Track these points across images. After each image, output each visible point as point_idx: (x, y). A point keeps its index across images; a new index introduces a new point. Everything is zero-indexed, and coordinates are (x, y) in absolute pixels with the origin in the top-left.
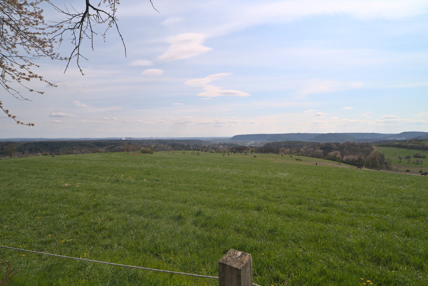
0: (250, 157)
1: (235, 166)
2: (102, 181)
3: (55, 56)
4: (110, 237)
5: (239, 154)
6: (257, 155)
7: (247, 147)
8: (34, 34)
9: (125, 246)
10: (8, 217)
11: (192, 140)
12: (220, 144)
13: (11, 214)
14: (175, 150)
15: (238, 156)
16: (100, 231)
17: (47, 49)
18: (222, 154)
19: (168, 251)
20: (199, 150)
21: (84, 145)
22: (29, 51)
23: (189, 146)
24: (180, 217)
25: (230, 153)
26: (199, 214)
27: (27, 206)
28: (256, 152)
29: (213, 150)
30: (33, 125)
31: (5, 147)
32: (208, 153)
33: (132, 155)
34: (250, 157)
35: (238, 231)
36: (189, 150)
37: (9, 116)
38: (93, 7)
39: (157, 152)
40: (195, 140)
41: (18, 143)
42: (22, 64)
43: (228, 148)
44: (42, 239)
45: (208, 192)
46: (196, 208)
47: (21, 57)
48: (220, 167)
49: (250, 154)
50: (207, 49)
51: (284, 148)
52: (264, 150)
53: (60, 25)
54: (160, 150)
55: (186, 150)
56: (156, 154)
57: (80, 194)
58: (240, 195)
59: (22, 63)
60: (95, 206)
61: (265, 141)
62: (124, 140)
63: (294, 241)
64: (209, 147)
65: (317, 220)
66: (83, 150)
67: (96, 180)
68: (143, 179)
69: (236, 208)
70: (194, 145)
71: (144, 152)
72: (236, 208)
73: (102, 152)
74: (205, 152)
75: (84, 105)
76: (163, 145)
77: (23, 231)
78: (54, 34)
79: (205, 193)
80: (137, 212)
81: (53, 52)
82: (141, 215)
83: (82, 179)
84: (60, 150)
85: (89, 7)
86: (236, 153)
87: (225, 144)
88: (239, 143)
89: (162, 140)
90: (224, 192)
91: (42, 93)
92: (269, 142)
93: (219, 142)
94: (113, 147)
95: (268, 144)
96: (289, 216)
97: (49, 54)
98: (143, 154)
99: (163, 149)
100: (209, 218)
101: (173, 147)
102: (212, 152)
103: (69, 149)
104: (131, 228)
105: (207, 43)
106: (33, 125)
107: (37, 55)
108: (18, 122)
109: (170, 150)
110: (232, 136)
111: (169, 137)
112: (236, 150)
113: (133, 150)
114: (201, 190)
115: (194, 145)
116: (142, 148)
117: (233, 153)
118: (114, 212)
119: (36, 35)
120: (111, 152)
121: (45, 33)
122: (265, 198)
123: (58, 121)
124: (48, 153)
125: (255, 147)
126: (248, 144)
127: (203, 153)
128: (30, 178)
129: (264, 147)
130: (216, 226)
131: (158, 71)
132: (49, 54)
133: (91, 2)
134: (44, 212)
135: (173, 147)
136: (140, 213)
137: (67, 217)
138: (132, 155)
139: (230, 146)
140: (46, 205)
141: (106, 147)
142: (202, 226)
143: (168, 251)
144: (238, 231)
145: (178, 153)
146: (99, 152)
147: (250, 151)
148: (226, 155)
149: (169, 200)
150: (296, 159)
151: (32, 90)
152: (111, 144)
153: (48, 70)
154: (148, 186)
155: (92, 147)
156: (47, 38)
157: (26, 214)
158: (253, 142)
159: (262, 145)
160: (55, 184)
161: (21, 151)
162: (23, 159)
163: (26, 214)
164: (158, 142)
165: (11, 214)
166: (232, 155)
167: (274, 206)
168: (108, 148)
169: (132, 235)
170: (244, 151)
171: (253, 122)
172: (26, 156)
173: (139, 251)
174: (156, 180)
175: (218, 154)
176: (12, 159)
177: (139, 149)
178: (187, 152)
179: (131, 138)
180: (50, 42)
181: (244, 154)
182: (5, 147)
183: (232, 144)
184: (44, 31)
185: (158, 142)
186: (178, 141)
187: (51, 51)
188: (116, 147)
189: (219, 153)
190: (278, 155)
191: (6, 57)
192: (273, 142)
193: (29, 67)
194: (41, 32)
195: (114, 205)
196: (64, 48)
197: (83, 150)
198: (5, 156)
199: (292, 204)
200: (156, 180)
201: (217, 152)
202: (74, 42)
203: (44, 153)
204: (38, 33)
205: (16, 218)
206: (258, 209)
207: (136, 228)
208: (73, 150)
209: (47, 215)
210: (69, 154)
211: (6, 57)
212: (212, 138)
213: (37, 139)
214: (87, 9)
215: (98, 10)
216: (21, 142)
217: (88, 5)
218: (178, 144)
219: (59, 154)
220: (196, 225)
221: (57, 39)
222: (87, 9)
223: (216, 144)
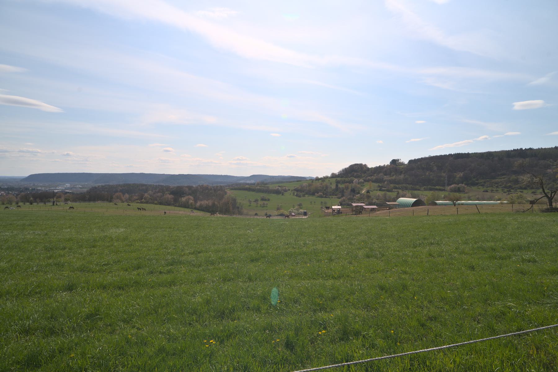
5: (42, 204)
7: (57, 193)
25: (21, 204)
35: (26, 332)
43: (17, 195)
49: (62, 204)
58: (36, 271)
61: (91, 184)
86: (35, 204)
88: (41, 187)
92: (97, 185)
95: (95, 188)
110: (26, 175)
117: (28, 204)
122: (82, 269)
126: (58, 189)
129: (89, 192)
139: (22, 191)
147: (63, 199)
158: (68, 185)
159: (85, 190)
170: (52, 200)
181: (51, 204)
183: (27, 189)
192: (103, 184)
206: (70, 288)
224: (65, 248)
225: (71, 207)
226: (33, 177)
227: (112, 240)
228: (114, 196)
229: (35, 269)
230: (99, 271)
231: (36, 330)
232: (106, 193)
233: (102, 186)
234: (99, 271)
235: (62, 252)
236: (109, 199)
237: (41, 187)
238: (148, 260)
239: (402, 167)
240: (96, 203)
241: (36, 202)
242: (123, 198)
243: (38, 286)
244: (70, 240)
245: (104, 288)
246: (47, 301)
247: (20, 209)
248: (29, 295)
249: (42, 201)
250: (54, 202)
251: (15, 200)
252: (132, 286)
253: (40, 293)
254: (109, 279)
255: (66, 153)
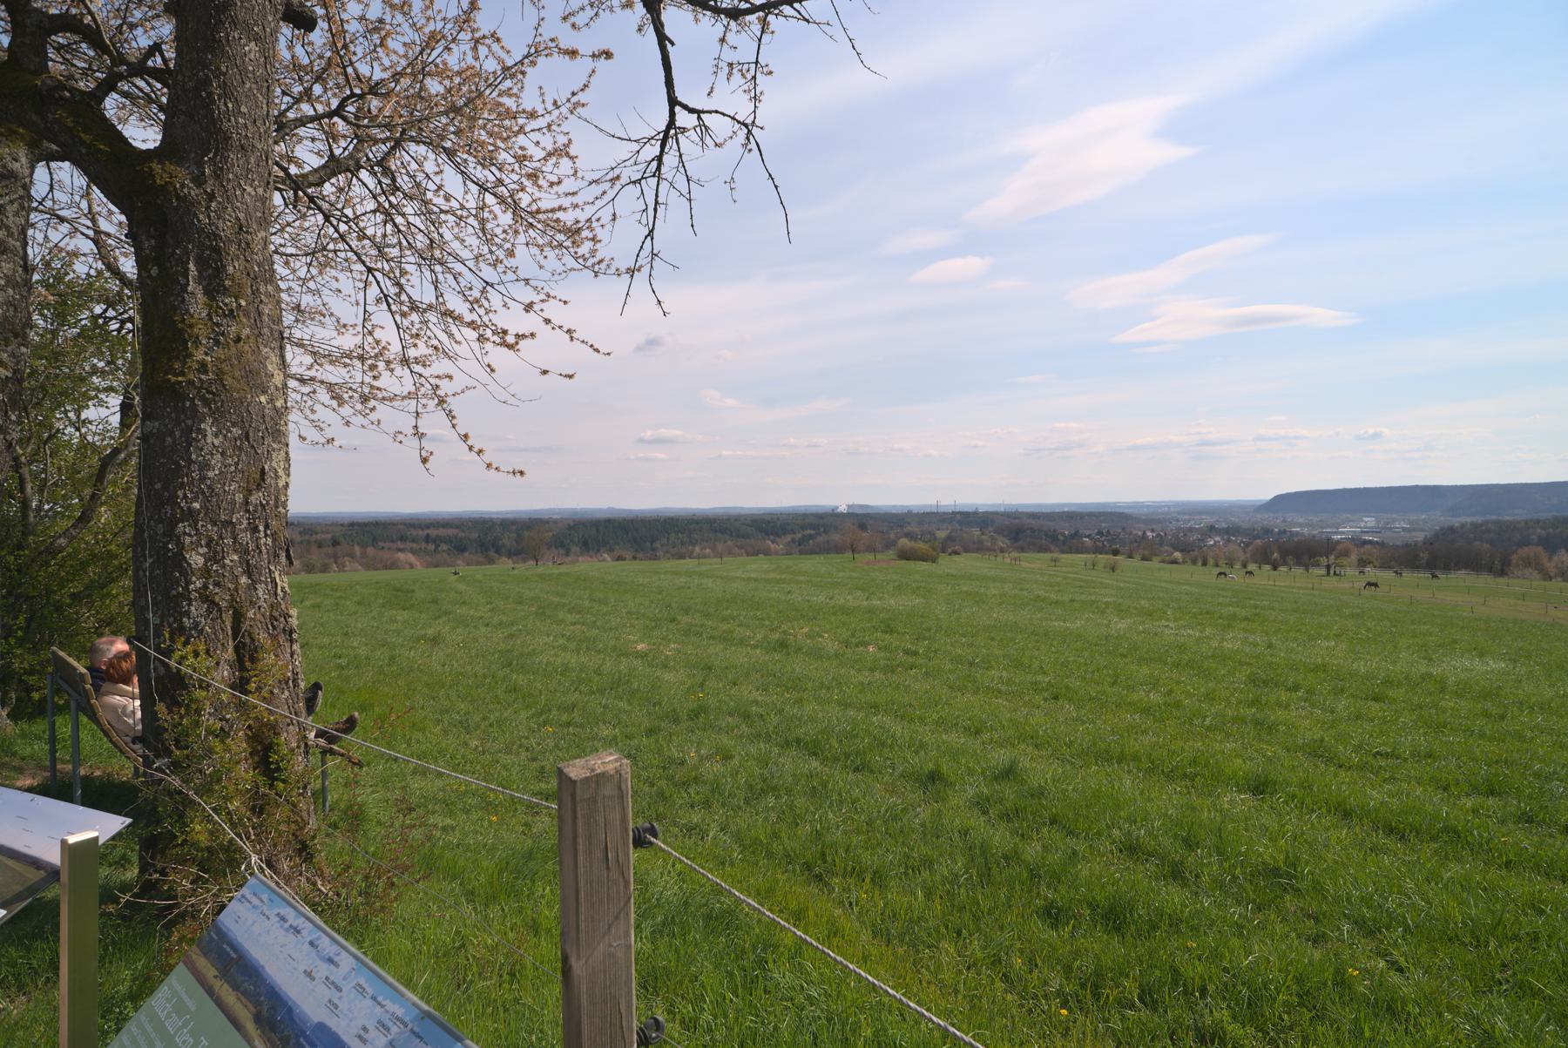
0: (1348, 585)
1: (1246, 619)
2: (742, 642)
3: (603, 266)
4: (707, 804)
5: (1299, 571)
6: (1385, 576)
7: (1338, 542)
8: (553, 211)
9: (738, 838)
10: (484, 719)
11: (1090, 514)
12: (1212, 530)
13: (490, 711)
14: (1022, 550)
15: (1291, 581)
16: (685, 784)
17: (585, 249)
18: (1216, 571)
19: (857, 873)
20: (1116, 553)
21: (723, 532)
22: (543, 262)
23: (1076, 534)
24: (934, 777)
25: (1252, 567)
26: (1008, 773)
27: (530, 695)
28: (1385, 565)
29: (1177, 555)
30: (522, 473)
31: (526, 534)
32: (1155, 563)
33: (868, 563)
34: (1348, 585)
35: (1132, 849)
36: (1078, 552)
37: (471, 448)
38: (685, 107)
39: (956, 558)
40: (1104, 514)
41: (555, 522)
42: (527, 301)
43: (1247, 545)
44: (543, 785)
45: (1079, 708)
46: (1001, 757)
47: (527, 281)
48: (1176, 620)
49: (1351, 572)
50: (1184, 151)
51: (1540, 549)
52: (1424, 556)
53: (610, 176)
54: (966, 551)
55: (1063, 552)
56: (948, 564)
57: (669, 677)
58: (1209, 728)
59: (527, 295)
60: (694, 715)
61: (1436, 519)
62: (842, 515)
63: (1359, 923)
64: (1161, 540)
65: (1537, 868)
66: (720, 547)
67: (726, 639)
68: (866, 644)
69: (1155, 769)
70: (1100, 533)
71: (906, 556)
72: (1155, 769)
73: (777, 553)
74: (1144, 559)
75: (730, 402)
76: (976, 532)
77: (508, 759)
78: (599, 203)
79: (1070, 708)
80: (806, 744)
81: (599, 256)
82: (815, 754)
83: (687, 633)
84: (657, 544)
85: (677, 109)
86: (1283, 569)
87: (1231, 531)
88: (1302, 526)
89: (975, 513)
90: (1146, 711)
91: (571, 377)
92: (1456, 522)
93: (1207, 520)
94: (811, 537)
95: (1452, 529)
96: (1390, 830)
97: (589, 263)
98: (903, 562)
99: (978, 548)
100: (1040, 793)
101: (1016, 539)
102: (1175, 562)
103: (683, 543)
104: (774, 789)
105: (1174, 129)
106: (522, 473)
107: (560, 269)
108: (489, 466)
109: (1002, 551)
110: (1268, 495)
111: (1167, 499)
112: (1285, 553)
113: (871, 549)
114: (1056, 698)
115: (1100, 533)
116: (904, 542)
117: (1267, 567)
118: (741, 737)
119: (560, 215)
120: (801, 553)
121: (577, 206)
122: (1316, 751)
123: (662, 456)
124: (628, 554)
125: (1382, 544)
126: (1345, 531)
127: (1136, 562)
128: (559, 622)
129: (1428, 543)
130: (1053, 821)
131: (971, 265)
132: (589, 263)
133: (680, 95)
134: (565, 717)
135: (1016, 539)
136: (813, 749)
137: (615, 738)
138: (868, 563)
139: (1255, 537)
140: (574, 697)
141: (789, 538)
142: (1006, 817)
143: (857, 873)
144: (1132, 849)
145: (1034, 562)
146: (767, 553)
147: (1354, 557)
148: (1236, 575)
149: (922, 720)
150: (1376, 585)
151: (545, 372)
152: (803, 528)
153: (589, 304)
154: (872, 670)
155: (745, 536)
156: (582, 216)
157: (524, 714)
158: (1370, 521)
159: (1420, 537)
160: (612, 643)
161: (562, 546)
162: (563, 569)
163: (524, 714)
164: (959, 522)
165: (490, 711)
166: (1264, 577)
167: (1341, 784)
168: (793, 541)
169: (767, 810)
170: (1323, 560)
171: (1376, 435)
172: (573, 562)
173: (770, 855)
174: (906, 652)
175: (1199, 568)
176: (540, 570)
177: (888, 545)
178: (1066, 558)
179: (867, 506)
180: (591, 228)
181: (1323, 571)
182: (526, 534)
183: (1267, 531)
184: (575, 200)
185: (959, 522)
186: (1034, 516)
187: (593, 252)
188: (820, 539)
189: (1205, 564)
190: (1502, 581)
191: (492, 286)
192: (1478, 519)
193: (543, 306)
194: (566, 202)
195: (746, 716)
196: (620, 242)
197: (720, 547)
198: (524, 561)
199: (1445, 789)
200: (906, 652)
201: (1194, 562)
202: (644, 221)
203: (617, 554)
204: (560, 208)
205: (500, 722)
206: (1260, 787)
207: (789, 791)
208: (694, 544)
209: (569, 724)
210: (682, 557)
211: (492, 286)
212: (1177, 504)
213: (600, 510)
214: (672, 114)
215: (698, 112)
216: (562, 520)
217: (673, 102)
218: (1032, 529)
219: (656, 558)
220: (985, 813)
221: (606, 216)
222: (672, 114)
223: (1191, 529)
224: (1296, 688)
225: (1369, 584)
226: (1284, 502)
227: (1443, 690)
228: (1515, 558)
229: (1207, 722)
230: (1362, 767)
231: (1151, 854)
232: (1487, 546)
233: (1475, 525)
234: (1362, 767)
235: (1284, 696)
236: (1501, 568)
237: (1300, 525)
238: (1537, 775)
239: (28, 782)
240: (1452, 575)
241: (1285, 563)
242: (1551, 566)
243: (1194, 762)
244: (1323, 668)
245: (1347, 814)
246: (1197, 802)
247: (1249, 580)
248: (1170, 776)
249: (1299, 564)
250: (1328, 567)
251: (1242, 557)
252: (1434, 838)
253: (1192, 778)
254: (1375, 796)
255: (1371, 431)
